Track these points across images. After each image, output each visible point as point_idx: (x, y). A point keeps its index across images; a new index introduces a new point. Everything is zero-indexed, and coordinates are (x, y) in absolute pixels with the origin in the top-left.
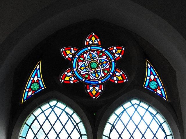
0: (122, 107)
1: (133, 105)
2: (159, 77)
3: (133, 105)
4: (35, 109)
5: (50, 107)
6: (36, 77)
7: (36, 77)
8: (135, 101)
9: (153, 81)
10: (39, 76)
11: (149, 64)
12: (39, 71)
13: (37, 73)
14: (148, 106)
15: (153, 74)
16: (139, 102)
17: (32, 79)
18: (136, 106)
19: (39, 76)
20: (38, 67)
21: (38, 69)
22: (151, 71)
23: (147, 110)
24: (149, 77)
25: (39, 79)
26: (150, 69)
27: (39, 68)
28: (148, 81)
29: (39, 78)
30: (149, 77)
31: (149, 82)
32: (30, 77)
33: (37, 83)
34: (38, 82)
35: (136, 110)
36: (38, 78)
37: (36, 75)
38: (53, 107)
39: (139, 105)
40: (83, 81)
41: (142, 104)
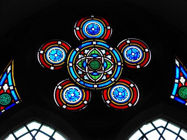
0: (53, 131)
1: (156, 129)
2: (15, 89)
3: (156, 129)
4: (3, 136)
5: (27, 131)
6: (6, 85)
7: (6, 85)
8: (160, 123)
9: (6, 93)
10: (10, 83)
11: (11, 68)
12: (10, 74)
13: (7, 78)
14: (25, 128)
15: (8, 84)
16: (166, 123)
17: (177, 81)
18: (161, 130)
19: (10, 83)
20: (9, 69)
21: (9, 73)
22: (180, 71)
23: (178, 135)
24: (178, 80)
25: (12, 88)
26: (179, 68)
27: (11, 71)
28: (176, 86)
29: (11, 86)
30: (178, 80)
31: (178, 89)
32: (58, 85)
33: (8, 94)
34: (8, 92)
35: (161, 136)
36: (8, 86)
37: (6, 81)
38: (34, 133)
39: (165, 128)
40: (96, 88)
41: (170, 126)
